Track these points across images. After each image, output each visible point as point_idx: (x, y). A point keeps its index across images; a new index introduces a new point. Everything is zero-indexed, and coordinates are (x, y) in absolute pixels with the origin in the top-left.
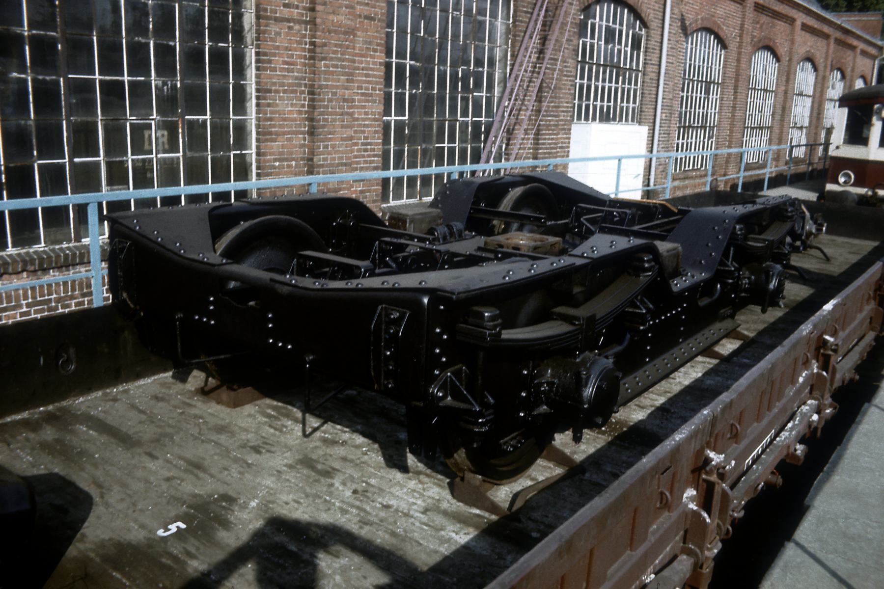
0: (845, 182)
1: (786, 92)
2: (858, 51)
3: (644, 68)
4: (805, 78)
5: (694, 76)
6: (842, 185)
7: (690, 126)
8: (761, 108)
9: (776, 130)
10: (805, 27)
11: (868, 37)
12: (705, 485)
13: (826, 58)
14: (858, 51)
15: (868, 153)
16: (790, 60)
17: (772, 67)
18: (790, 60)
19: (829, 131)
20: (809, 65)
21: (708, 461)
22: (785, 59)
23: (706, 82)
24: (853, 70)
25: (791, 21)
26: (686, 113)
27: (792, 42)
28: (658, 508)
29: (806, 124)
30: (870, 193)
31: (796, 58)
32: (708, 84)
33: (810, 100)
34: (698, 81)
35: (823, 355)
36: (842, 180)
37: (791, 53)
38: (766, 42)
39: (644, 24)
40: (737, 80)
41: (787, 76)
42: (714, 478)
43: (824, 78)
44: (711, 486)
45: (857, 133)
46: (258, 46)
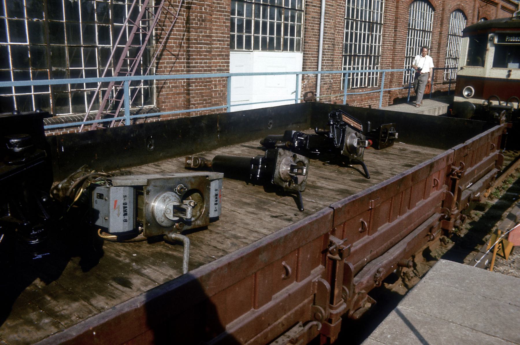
0: (468, 95)
2: (500, 6)
3: (306, 8)
5: (357, 17)
6: (467, 97)
7: (355, 56)
14: (500, 6)
15: (484, 73)
17: (429, 14)
18: (443, 9)
22: (439, 9)
23: (369, 22)
26: (351, 45)
28: (361, 232)
30: (486, 103)
34: (361, 21)
36: (465, 93)
40: (396, 22)
41: (442, 21)
42: (337, 257)
45: (476, 57)
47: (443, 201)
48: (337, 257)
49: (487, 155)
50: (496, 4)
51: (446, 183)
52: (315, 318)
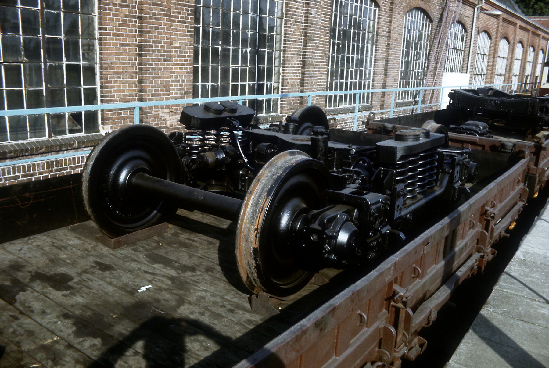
1: (512, 58)
2: (541, 37)
4: (519, 51)
8: (501, 66)
9: (507, 76)
10: (521, 28)
11: (545, 30)
12: (393, 309)
13: (528, 42)
14: (541, 37)
16: (514, 43)
17: (487, 42)
19: (527, 77)
20: (520, 45)
21: (395, 293)
22: (512, 42)
24: (538, 46)
25: (515, 24)
27: (515, 34)
28: (414, 277)
29: (518, 74)
31: (517, 41)
32: (484, 55)
33: (531, 63)
35: (485, 219)
37: (514, 39)
38: (486, 29)
39: (466, 31)
41: (512, 51)
42: (400, 305)
43: (527, 51)
44: (398, 310)
46: (376, 45)
47: (478, 240)
48: (400, 305)
49: (513, 189)
50: (473, 6)
51: (480, 221)
52: (381, 360)
